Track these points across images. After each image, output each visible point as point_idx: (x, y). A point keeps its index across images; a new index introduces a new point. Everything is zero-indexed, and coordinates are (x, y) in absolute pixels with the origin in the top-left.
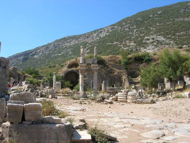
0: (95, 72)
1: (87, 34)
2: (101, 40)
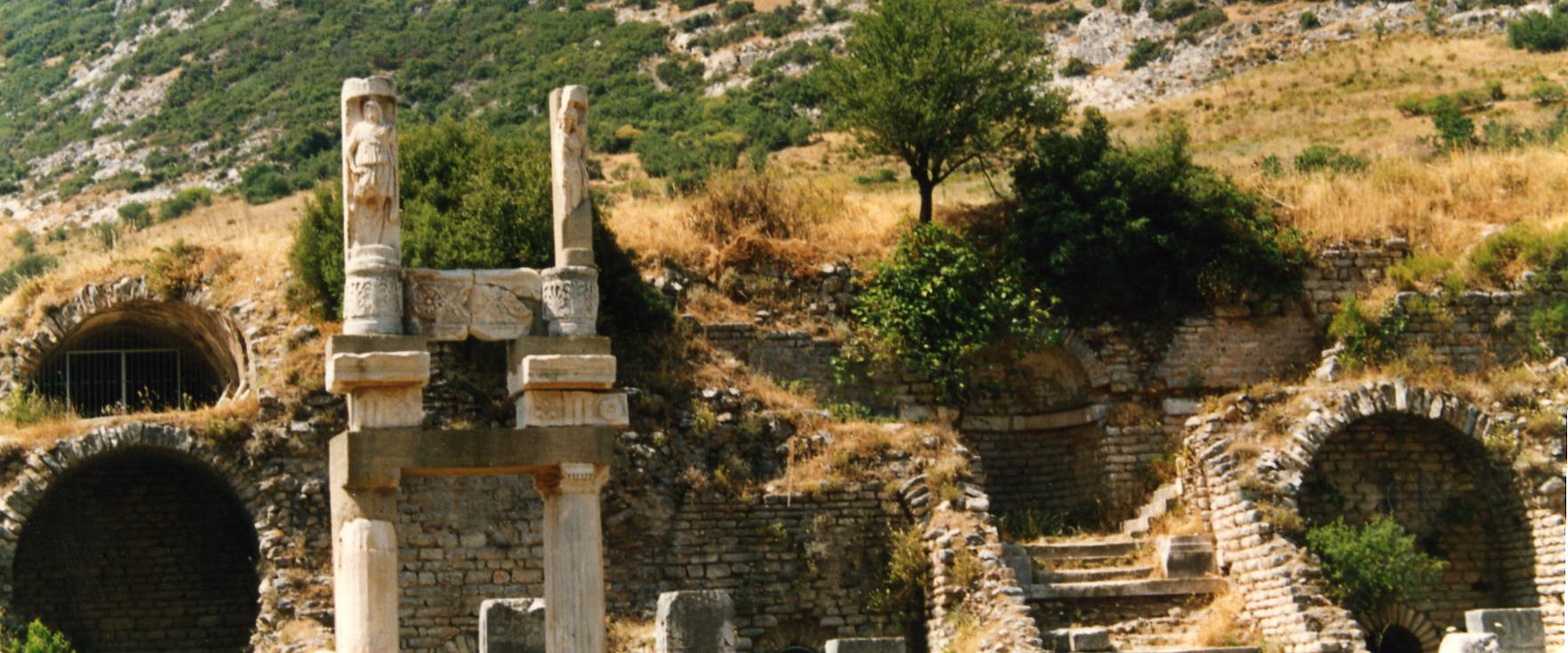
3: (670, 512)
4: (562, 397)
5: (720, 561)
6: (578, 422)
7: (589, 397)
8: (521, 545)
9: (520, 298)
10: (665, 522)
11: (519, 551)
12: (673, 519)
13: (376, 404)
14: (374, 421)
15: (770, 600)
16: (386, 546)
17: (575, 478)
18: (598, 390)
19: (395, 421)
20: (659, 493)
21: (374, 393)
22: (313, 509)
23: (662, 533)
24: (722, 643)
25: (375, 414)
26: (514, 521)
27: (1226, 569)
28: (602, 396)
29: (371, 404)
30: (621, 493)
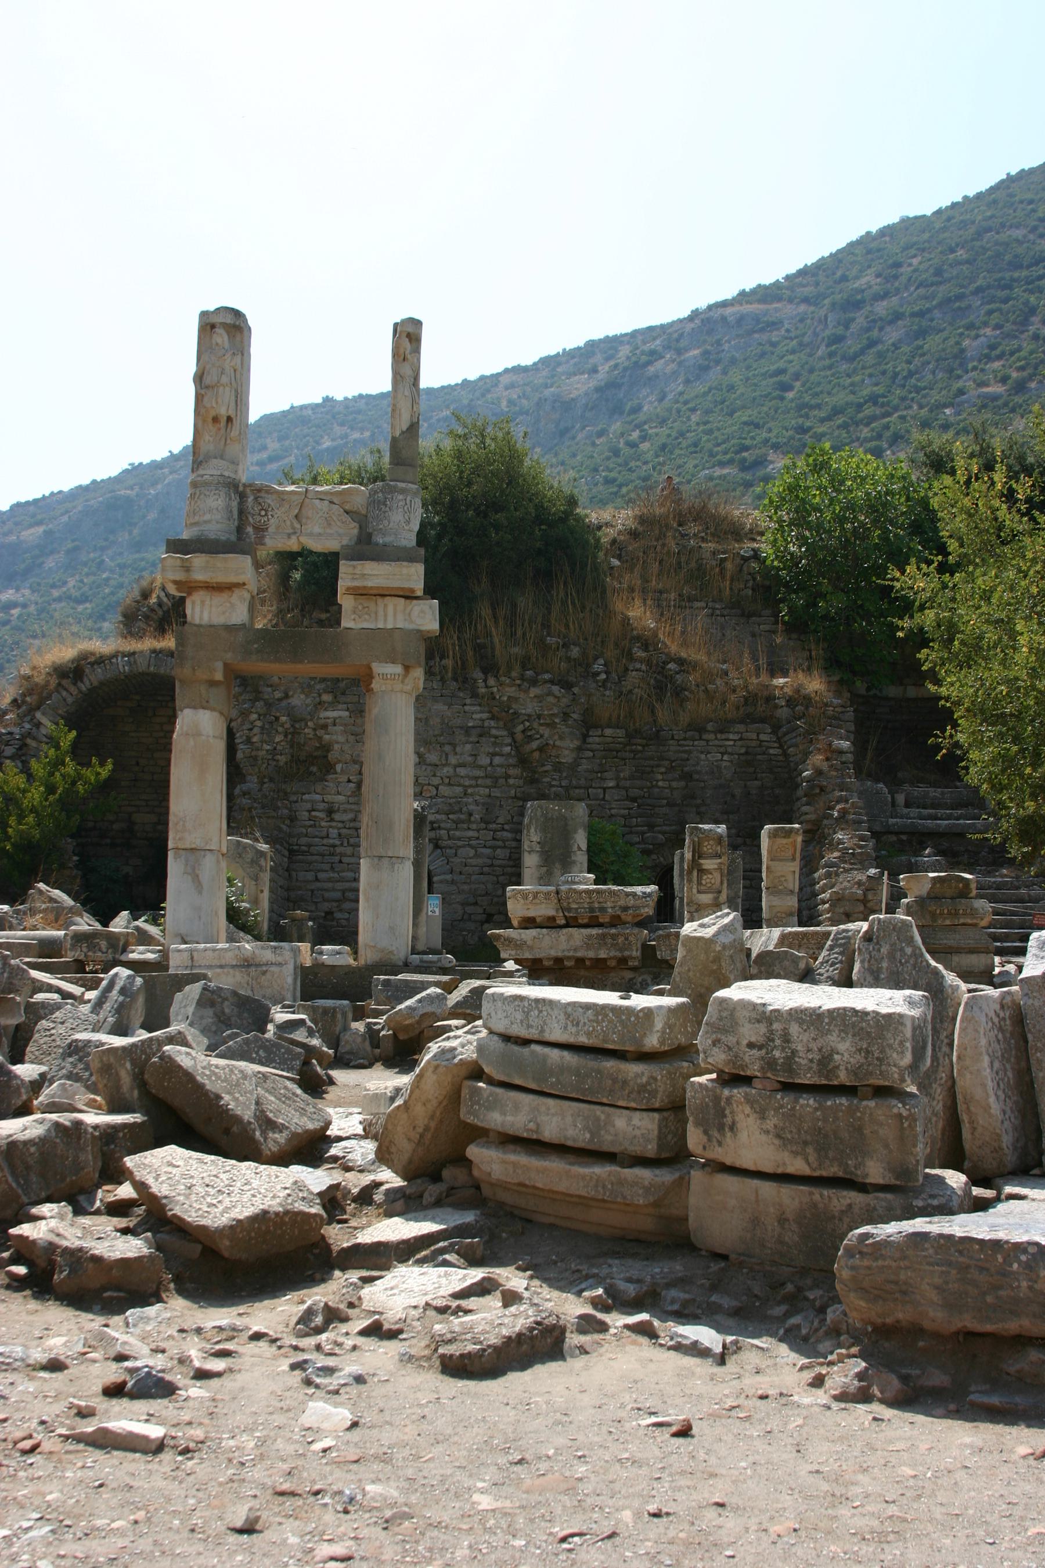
0: (378, 668)
1: (505, 380)
2: (644, 438)
3: (577, 743)
5: (617, 786)
6: (390, 626)
7: (402, 600)
8: (446, 765)
9: (347, 512)
10: (572, 750)
11: (445, 770)
12: (579, 749)
13: (203, 602)
14: (201, 619)
15: (659, 821)
16: (211, 733)
17: (384, 677)
18: (408, 596)
19: (219, 620)
20: (567, 726)
21: (202, 593)
22: (280, 729)
23: (570, 761)
24: (575, 848)
25: (202, 612)
26: (442, 745)
27: (341, 464)
28: (415, 602)
29: (198, 602)
30: (535, 725)
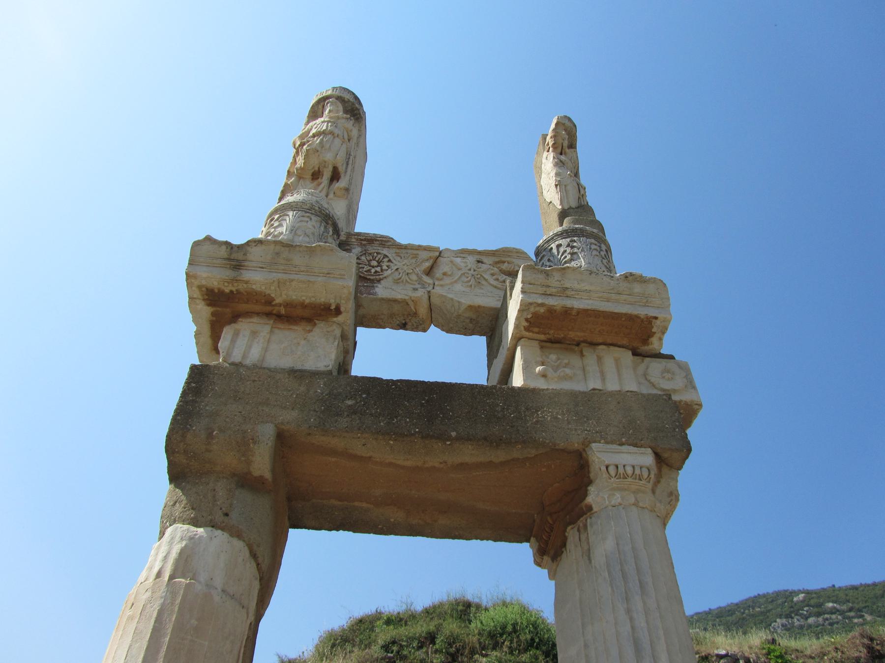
4: (582, 355)
21: (255, 320)
